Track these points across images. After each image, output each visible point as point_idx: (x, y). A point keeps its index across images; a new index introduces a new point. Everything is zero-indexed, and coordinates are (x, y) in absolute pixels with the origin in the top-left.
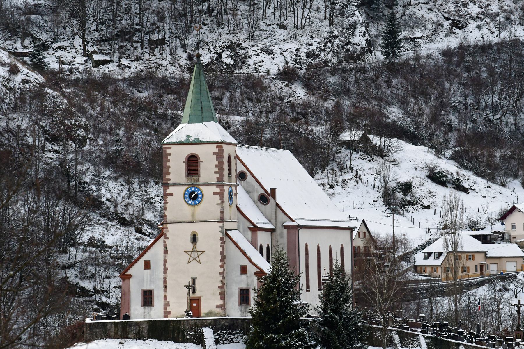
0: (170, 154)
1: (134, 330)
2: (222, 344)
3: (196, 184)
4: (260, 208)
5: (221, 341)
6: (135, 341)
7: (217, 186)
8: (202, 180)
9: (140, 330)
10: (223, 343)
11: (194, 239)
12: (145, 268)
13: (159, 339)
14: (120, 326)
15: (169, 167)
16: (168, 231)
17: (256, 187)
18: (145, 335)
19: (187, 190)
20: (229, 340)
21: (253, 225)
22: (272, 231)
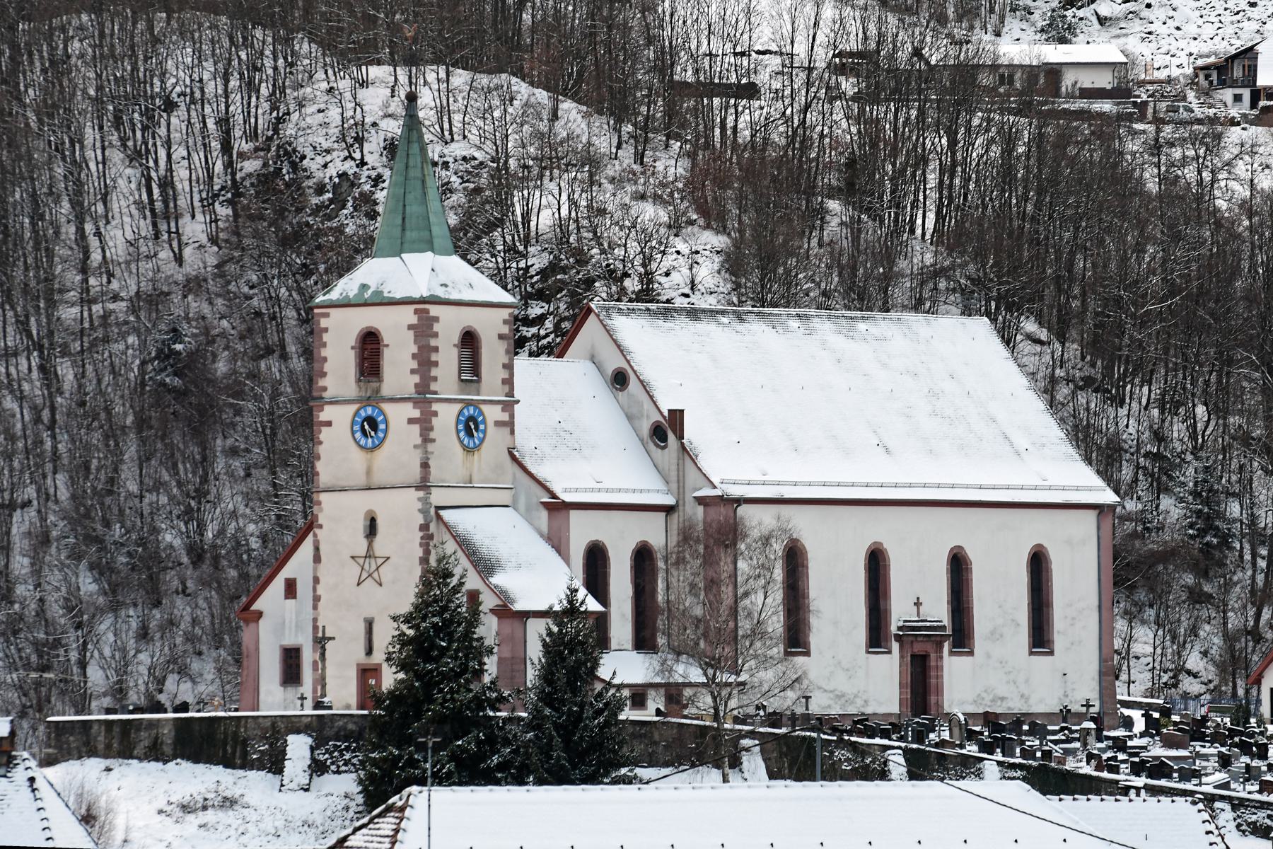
0: (326, 330)
1: (144, 739)
2: (335, 773)
3: (374, 399)
4: (653, 455)
5: (333, 768)
6: (145, 764)
7: (416, 403)
8: (386, 390)
9: (157, 738)
10: (338, 772)
11: (372, 528)
12: (287, 597)
13: (196, 761)
14: (116, 729)
15: (325, 359)
16: (321, 510)
17: (645, 407)
18: (168, 750)
19: (356, 413)
20: (354, 765)
21: (554, 496)
22: (668, 510)
